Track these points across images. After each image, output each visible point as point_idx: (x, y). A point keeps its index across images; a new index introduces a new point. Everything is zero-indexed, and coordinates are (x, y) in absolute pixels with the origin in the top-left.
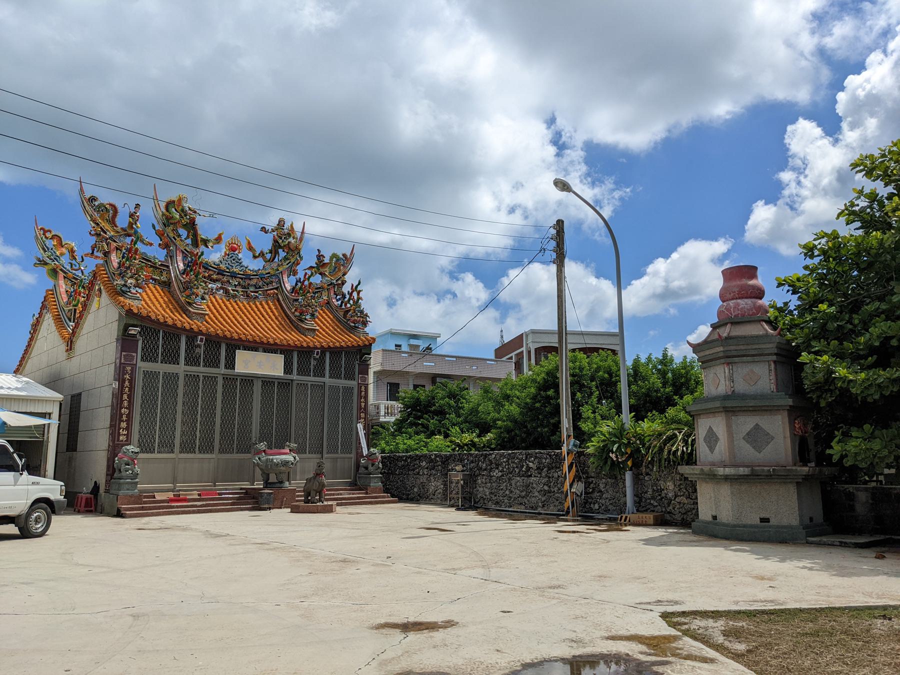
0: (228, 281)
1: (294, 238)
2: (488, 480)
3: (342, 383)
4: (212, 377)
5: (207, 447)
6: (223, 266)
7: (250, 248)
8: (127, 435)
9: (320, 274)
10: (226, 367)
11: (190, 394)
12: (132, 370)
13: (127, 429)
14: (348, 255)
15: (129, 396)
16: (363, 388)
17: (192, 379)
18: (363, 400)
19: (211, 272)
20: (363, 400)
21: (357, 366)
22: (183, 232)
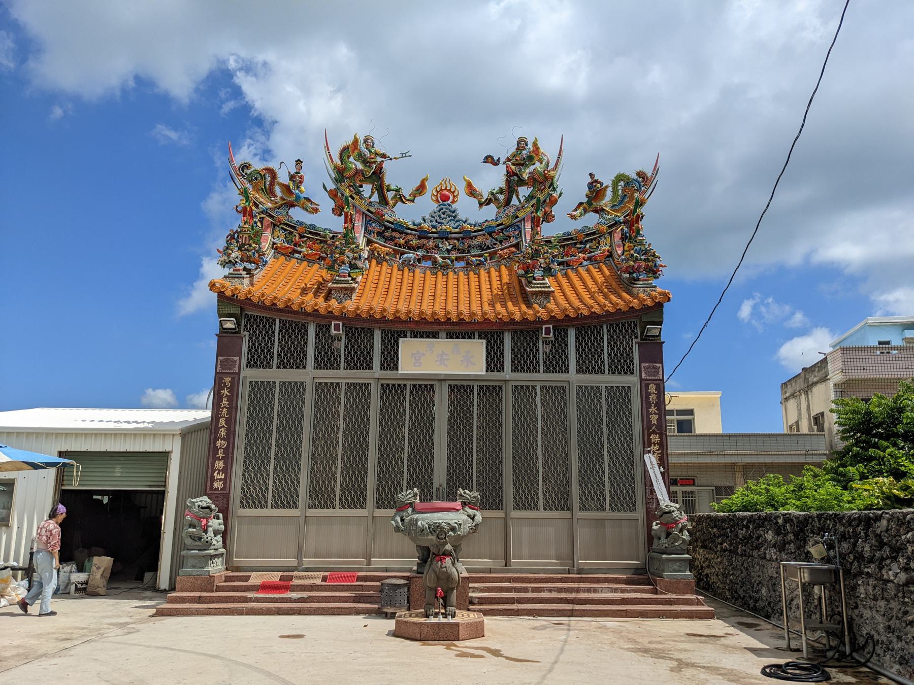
0: (437, 246)
1: (540, 161)
2: (878, 591)
3: (606, 380)
4: (361, 385)
5: (354, 498)
6: (426, 226)
7: (472, 192)
8: (225, 480)
9: (596, 211)
10: (383, 367)
11: (324, 414)
12: (232, 382)
13: (225, 470)
14: (649, 175)
15: (228, 421)
16: (652, 388)
17: (325, 391)
18: (653, 409)
19: (410, 237)
20: (653, 409)
21: (636, 349)
22: (367, 189)
